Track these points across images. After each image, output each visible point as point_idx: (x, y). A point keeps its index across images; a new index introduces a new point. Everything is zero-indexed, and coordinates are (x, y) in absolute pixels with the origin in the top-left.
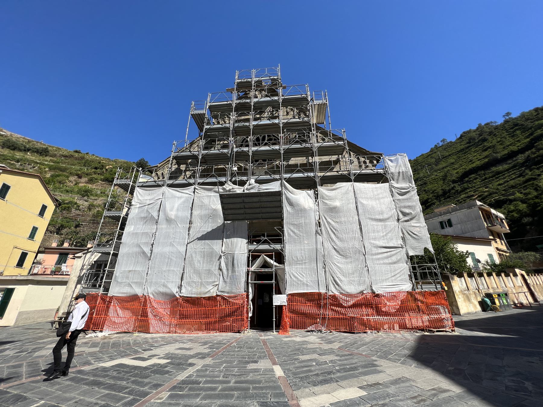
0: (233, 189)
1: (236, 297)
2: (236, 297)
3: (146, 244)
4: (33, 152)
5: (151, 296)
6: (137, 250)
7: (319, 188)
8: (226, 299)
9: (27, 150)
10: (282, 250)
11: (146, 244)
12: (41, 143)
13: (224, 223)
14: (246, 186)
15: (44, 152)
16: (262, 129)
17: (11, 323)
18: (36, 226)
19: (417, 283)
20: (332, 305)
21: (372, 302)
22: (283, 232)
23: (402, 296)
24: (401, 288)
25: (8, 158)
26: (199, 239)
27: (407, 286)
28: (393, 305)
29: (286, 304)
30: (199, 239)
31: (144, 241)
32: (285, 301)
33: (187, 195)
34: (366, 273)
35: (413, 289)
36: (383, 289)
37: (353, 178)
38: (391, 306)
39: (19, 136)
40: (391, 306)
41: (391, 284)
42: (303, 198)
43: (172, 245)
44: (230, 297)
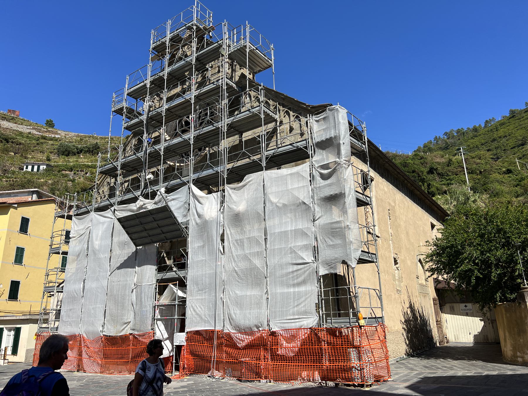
0: (144, 204)
1: (144, 335)
2: (144, 335)
3: (305, 247)
4: (86, 152)
5: (85, 336)
6: (243, 265)
7: (227, 187)
8: (136, 338)
9: (80, 151)
10: (184, 277)
11: (305, 247)
12: (93, 137)
13: (137, 249)
14: (157, 198)
15: (94, 150)
16: (182, 109)
17: (23, 360)
18: (17, 267)
19: (328, 315)
20: (226, 346)
21: (265, 343)
22: (187, 254)
23: (303, 335)
24: (302, 323)
25: (63, 168)
26: (119, 268)
27: (312, 321)
28: (290, 347)
29: (185, 344)
30: (119, 268)
31: (301, 243)
32: (184, 340)
33: (109, 219)
34: (265, 301)
35: (319, 324)
36: (282, 325)
37: (264, 164)
38: (287, 348)
39: (73, 134)
40: (287, 348)
41: (292, 317)
42: (209, 205)
43: (97, 279)
44: (139, 335)
